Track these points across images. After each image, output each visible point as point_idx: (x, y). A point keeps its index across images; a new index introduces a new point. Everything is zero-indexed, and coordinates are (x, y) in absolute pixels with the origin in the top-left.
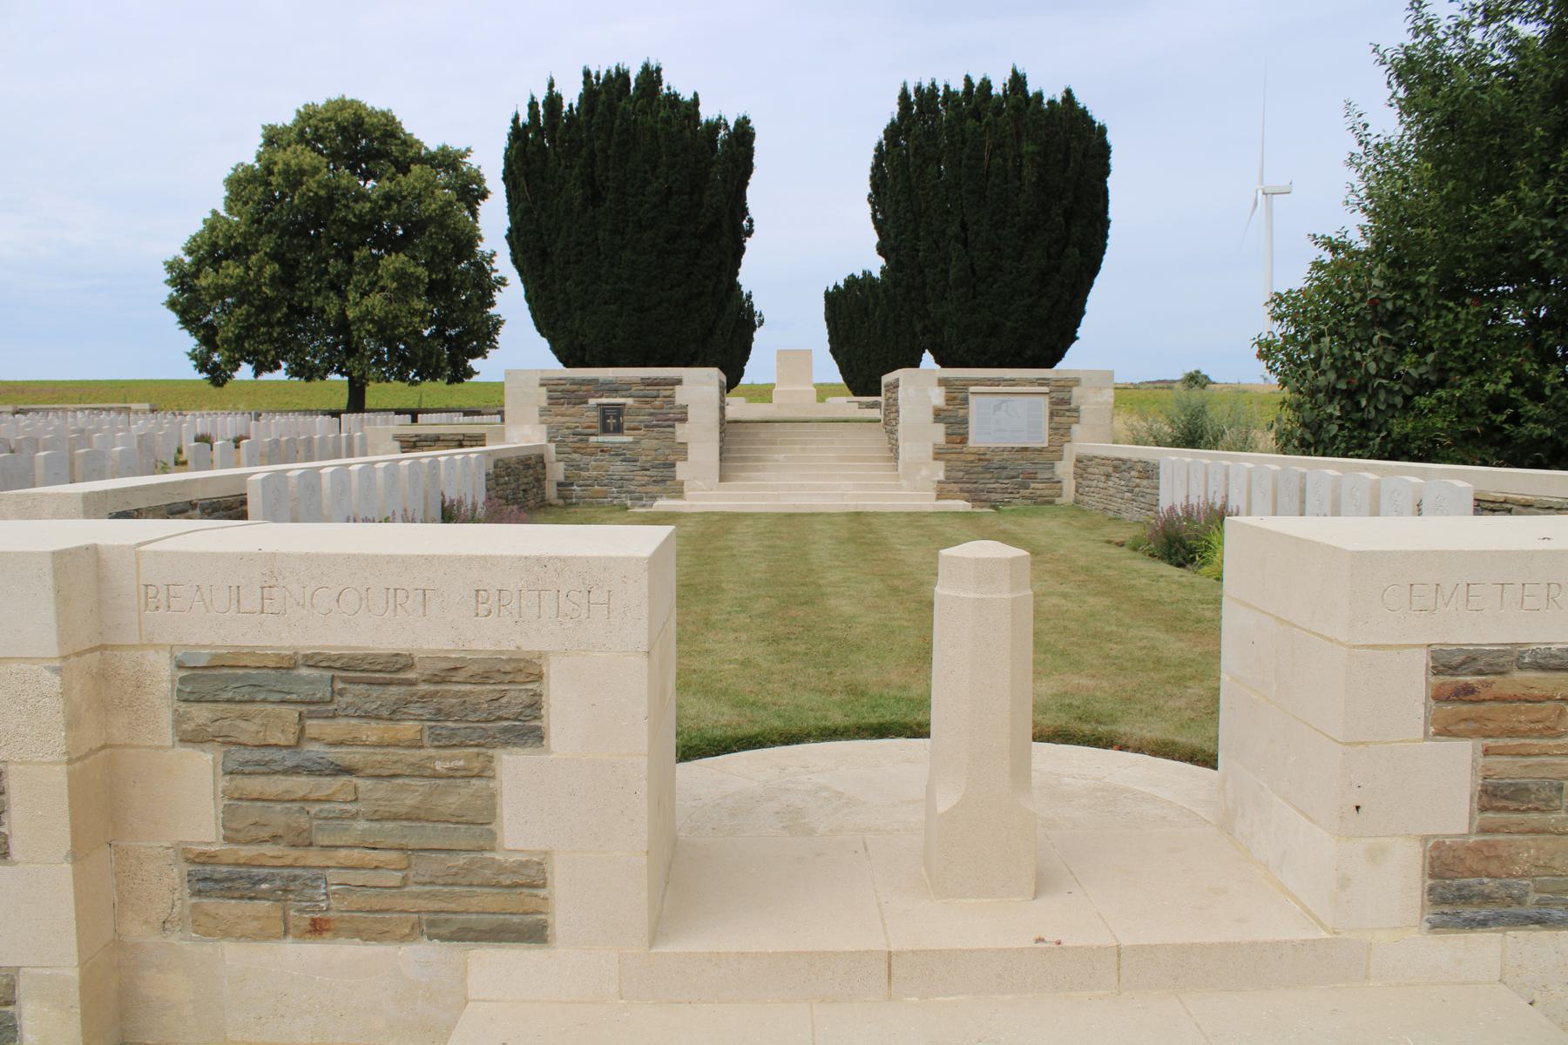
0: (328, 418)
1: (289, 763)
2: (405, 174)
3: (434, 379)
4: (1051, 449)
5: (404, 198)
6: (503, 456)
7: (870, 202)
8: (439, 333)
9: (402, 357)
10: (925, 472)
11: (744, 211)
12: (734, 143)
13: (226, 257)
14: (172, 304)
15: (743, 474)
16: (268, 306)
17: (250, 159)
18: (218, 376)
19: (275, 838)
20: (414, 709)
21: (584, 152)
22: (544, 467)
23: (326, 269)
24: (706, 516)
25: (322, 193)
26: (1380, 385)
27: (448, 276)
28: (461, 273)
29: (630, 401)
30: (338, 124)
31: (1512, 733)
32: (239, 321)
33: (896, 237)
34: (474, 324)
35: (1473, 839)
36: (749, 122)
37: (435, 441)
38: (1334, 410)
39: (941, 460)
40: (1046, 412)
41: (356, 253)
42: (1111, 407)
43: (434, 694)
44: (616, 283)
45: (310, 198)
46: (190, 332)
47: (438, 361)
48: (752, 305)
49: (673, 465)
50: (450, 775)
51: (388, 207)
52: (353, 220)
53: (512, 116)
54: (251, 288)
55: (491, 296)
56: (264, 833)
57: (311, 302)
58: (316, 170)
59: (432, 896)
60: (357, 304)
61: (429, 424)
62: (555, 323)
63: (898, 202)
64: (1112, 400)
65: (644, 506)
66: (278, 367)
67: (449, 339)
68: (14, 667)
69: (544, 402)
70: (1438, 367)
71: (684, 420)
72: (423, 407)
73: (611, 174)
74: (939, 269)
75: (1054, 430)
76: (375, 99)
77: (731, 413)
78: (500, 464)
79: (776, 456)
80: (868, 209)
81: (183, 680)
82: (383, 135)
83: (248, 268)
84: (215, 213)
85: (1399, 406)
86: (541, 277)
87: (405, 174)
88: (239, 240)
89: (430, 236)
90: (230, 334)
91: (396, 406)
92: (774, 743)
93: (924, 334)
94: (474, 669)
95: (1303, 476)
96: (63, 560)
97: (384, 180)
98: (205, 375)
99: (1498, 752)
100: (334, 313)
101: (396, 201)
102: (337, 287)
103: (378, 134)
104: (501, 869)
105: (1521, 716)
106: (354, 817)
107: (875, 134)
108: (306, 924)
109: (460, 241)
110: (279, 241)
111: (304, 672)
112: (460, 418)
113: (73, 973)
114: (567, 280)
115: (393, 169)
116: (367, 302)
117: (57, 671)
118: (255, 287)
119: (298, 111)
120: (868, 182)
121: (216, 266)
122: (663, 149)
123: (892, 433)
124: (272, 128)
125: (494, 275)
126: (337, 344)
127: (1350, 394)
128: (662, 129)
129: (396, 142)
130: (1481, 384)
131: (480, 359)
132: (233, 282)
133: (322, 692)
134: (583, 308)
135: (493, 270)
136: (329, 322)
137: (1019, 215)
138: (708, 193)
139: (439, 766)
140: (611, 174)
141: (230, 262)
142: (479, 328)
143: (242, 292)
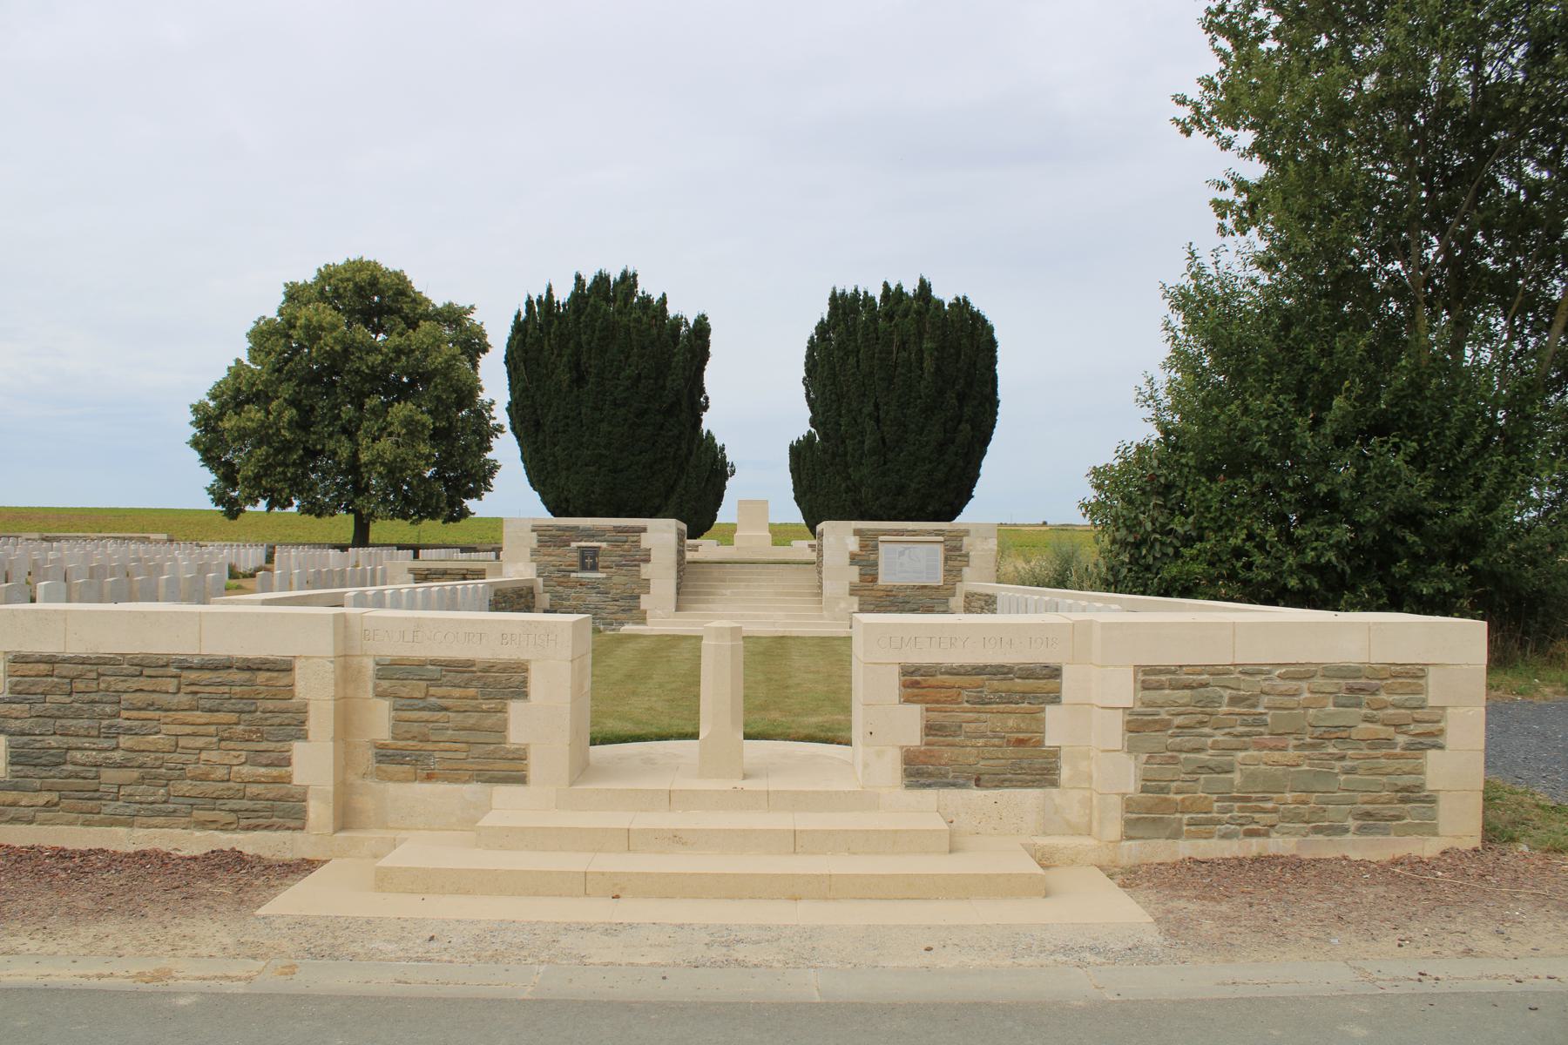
0: (338, 552)
1: (421, 705)
2: (414, 330)
3: (433, 518)
4: (946, 587)
5: (413, 351)
6: (501, 587)
7: (805, 384)
8: (439, 476)
9: (405, 497)
10: (843, 605)
11: (702, 390)
12: (693, 338)
13: (248, 401)
14: (195, 443)
15: (704, 606)
16: (287, 447)
17: (272, 314)
18: (233, 510)
19: (414, 738)
20: (475, 683)
21: (572, 344)
22: (533, 597)
23: (339, 415)
24: (660, 638)
25: (338, 348)
26: (1156, 539)
27: (451, 424)
28: (463, 420)
29: (604, 545)
30: (356, 284)
31: (937, 702)
32: (259, 461)
33: (823, 414)
34: (472, 468)
35: (923, 748)
36: (707, 319)
37: (443, 574)
38: (1125, 558)
39: (856, 595)
40: (941, 557)
41: (367, 400)
42: (994, 553)
43: (483, 677)
44: (594, 449)
45: (326, 352)
46: (211, 469)
47: (438, 502)
48: (725, 457)
49: (639, 597)
50: (487, 711)
51: (398, 359)
52: (366, 371)
53: (515, 313)
54: (270, 432)
55: (489, 441)
56: (408, 736)
57: (324, 445)
58: (334, 327)
59: (479, 763)
60: (368, 448)
61: (430, 559)
62: (546, 479)
63: (825, 386)
64: (996, 548)
65: (613, 630)
66: (291, 504)
67: (446, 481)
68: (315, 660)
69: (534, 544)
70: (1198, 526)
71: (647, 561)
72: (422, 542)
73: (592, 362)
74: (856, 441)
75: (948, 571)
76: (390, 261)
77: (689, 556)
78: (499, 593)
79: (724, 591)
80: (803, 389)
81: (378, 670)
82: (395, 294)
83: (268, 413)
84: (238, 361)
85: (1171, 555)
86: (535, 443)
87: (414, 330)
88: (260, 387)
89: (436, 387)
90: (250, 473)
91: (395, 541)
92: (652, 740)
93: (846, 493)
94: (500, 666)
95: (1026, 599)
96: (336, 615)
97: (394, 334)
98: (220, 508)
99: (933, 710)
100: (345, 455)
101: (404, 354)
102: (349, 432)
103: (391, 293)
104: (508, 751)
105: (943, 694)
106: (447, 729)
107: (809, 330)
108: (424, 775)
109: (463, 392)
110: (297, 389)
111: (430, 667)
112: (457, 554)
113: (331, 788)
114: (555, 445)
115: (403, 325)
116: (379, 445)
117: (331, 662)
118: (274, 430)
119: (319, 270)
120: (803, 368)
121: (238, 411)
122: (635, 343)
123: (820, 573)
124: (294, 285)
125: (492, 422)
126: (346, 484)
127: (1137, 545)
128: (634, 327)
129: (407, 300)
130: (1226, 539)
131: (475, 500)
132: (254, 425)
133: (437, 675)
134: (568, 469)
135: (491, 418)
136: (340, 464)
137: (920, 398)
138: (670, 378)
139: (484, 707)
140: (592, 362)
141: (251, 406)
142: (477, 471)
143: (262, 436)
